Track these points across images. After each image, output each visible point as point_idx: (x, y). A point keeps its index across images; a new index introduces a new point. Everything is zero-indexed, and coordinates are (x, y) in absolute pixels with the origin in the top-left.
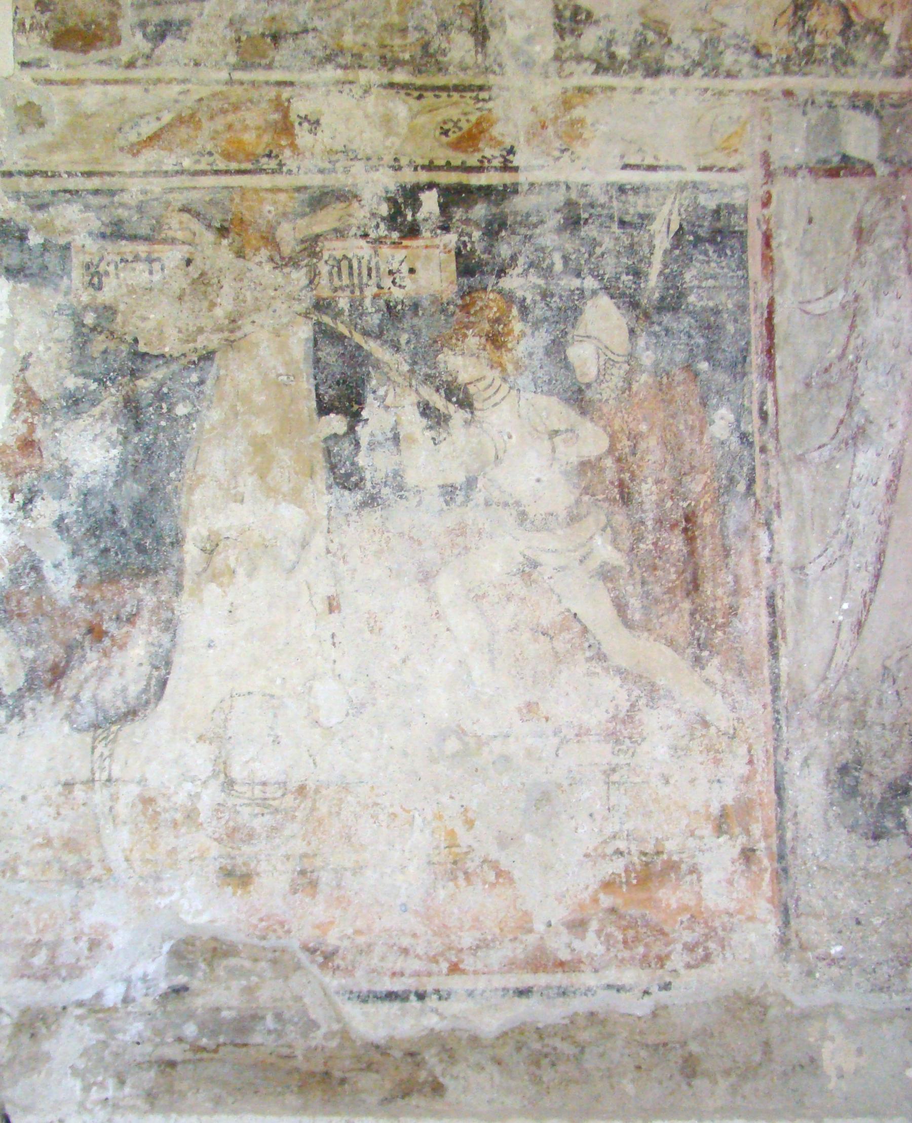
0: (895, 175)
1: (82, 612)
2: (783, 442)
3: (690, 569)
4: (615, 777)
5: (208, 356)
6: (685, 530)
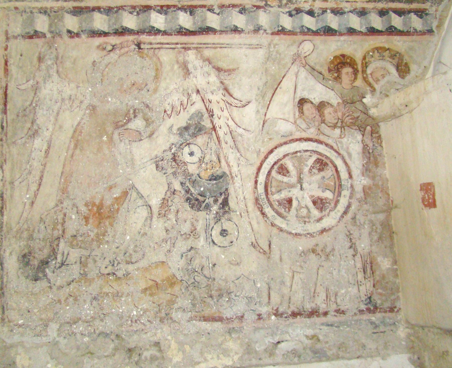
0: (53, 37)
2: (8, 137)
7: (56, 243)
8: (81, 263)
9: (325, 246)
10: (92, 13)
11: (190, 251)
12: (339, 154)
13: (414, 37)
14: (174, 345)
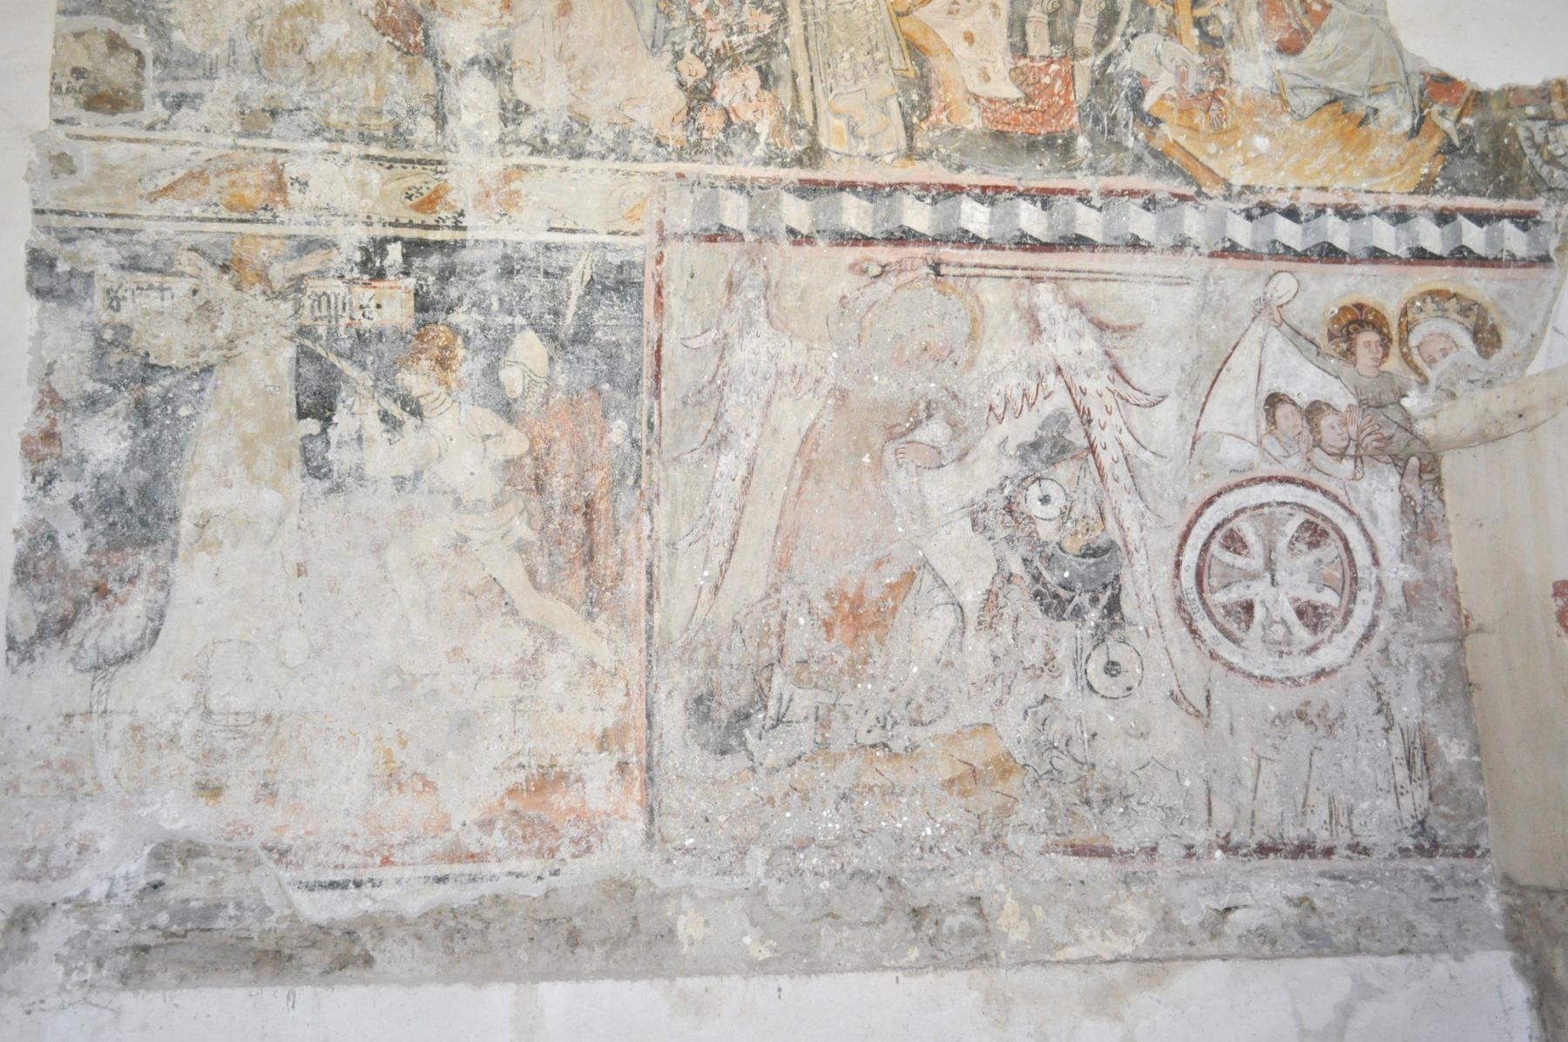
1: (91, 574)
3: (587, 544)
4: (521, 706)
5: (208, 369)
6: (585, 514)
7: (766, 674)
8: (817, 719)
9: (1325, 707)
10: (839, 195)
11: (1042, 703)
12: (1352, 513)
13: (1511, 272)
14: (1010, 904)
